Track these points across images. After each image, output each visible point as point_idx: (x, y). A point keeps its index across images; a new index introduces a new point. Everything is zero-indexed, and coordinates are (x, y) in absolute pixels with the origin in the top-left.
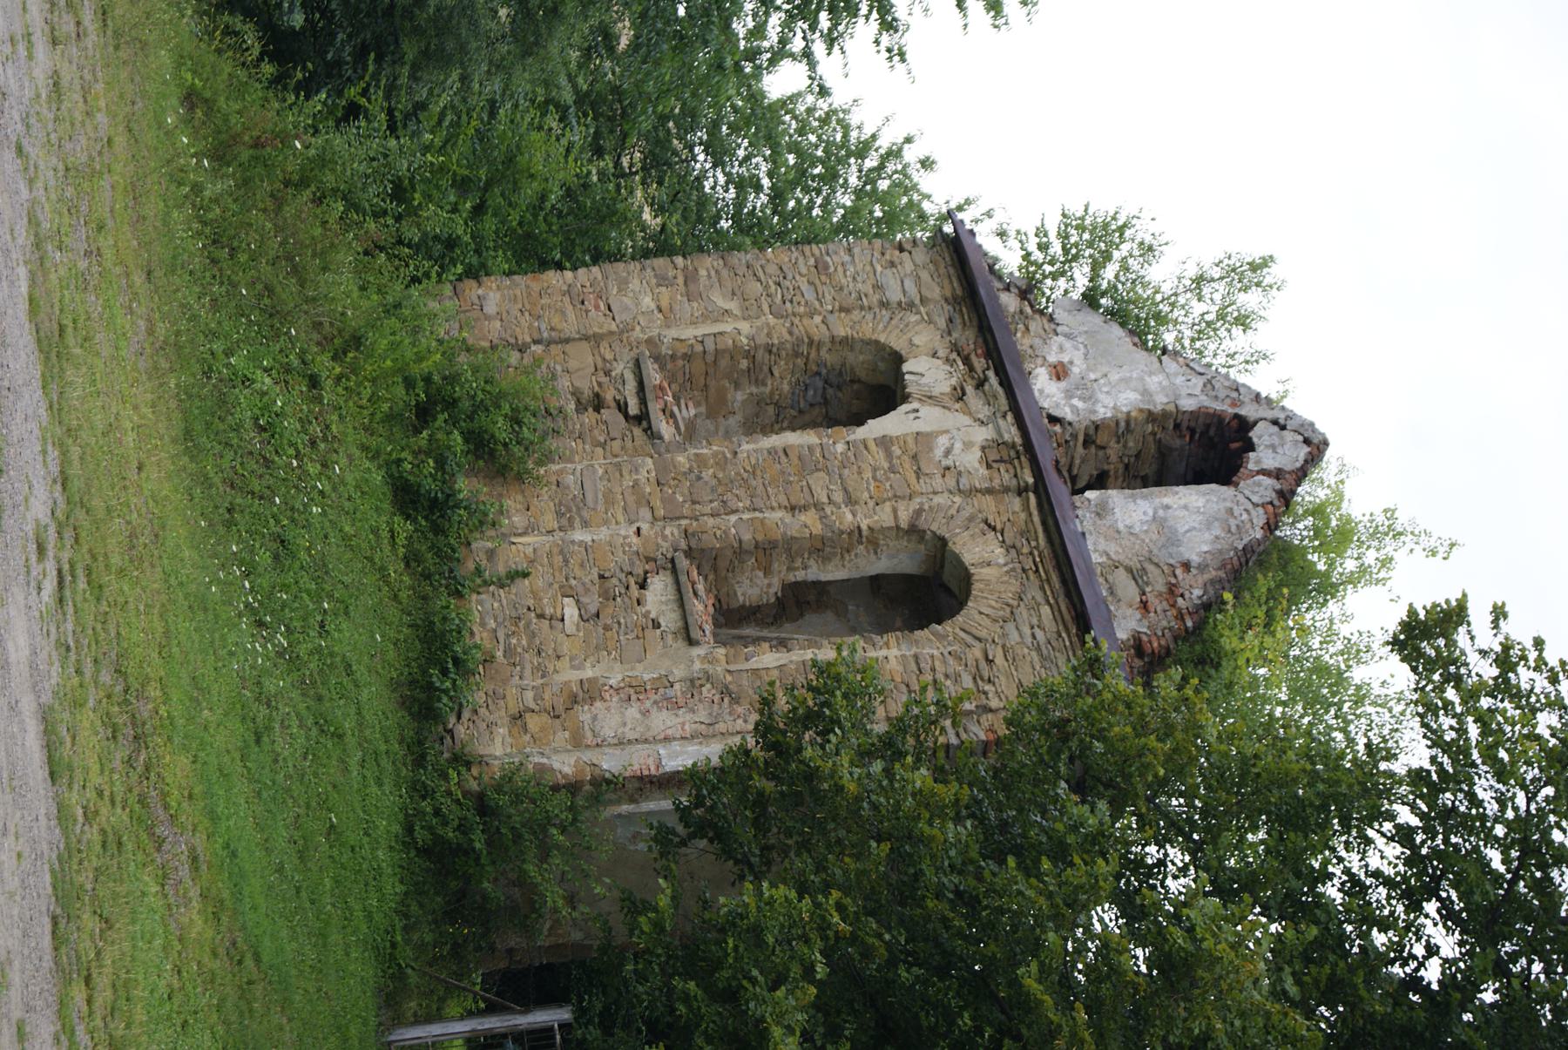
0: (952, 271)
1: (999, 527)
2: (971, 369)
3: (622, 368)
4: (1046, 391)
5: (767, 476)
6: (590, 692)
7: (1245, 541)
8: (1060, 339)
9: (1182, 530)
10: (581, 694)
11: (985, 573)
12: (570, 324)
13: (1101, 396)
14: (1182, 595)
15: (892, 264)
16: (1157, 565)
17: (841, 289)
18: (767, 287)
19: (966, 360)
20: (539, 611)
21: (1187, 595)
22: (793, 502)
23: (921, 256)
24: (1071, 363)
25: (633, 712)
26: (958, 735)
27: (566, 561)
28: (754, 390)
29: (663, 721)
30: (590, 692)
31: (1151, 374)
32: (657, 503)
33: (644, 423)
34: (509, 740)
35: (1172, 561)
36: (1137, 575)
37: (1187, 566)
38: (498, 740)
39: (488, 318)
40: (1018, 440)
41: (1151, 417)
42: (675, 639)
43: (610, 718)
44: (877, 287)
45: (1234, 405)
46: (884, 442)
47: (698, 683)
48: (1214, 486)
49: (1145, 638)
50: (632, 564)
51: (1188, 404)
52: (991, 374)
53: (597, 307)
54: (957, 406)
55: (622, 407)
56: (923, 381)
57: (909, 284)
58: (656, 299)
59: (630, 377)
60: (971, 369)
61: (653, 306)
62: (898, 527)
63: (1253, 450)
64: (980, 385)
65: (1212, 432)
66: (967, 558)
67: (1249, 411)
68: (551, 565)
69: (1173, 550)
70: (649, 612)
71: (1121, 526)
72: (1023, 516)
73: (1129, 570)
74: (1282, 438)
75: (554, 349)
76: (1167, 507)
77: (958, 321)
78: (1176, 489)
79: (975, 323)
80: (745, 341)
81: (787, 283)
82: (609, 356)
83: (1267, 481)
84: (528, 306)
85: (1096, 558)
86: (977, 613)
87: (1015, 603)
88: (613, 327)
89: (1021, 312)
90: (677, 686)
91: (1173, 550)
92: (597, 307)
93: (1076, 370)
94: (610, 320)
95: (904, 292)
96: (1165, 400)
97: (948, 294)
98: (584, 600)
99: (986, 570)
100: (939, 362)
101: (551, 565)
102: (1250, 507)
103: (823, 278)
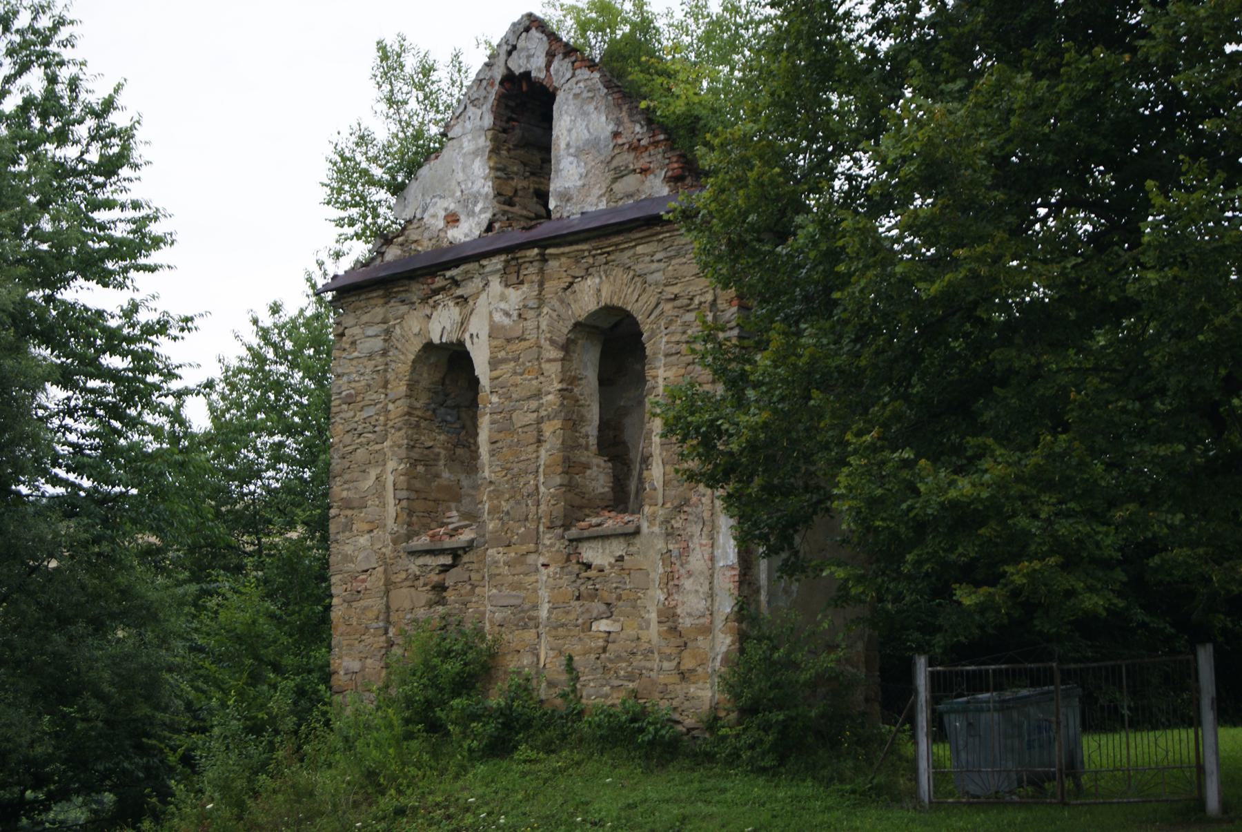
0: (363, 297)
3: (414, 566)
4: (466, 231)
6: (669, 616)
7: (601, 86)
9: (587, 135)
12: (375, 603)
13: (475, 188)
14: (639, 140)
15: (353, 343)
16: (613, 158)
17: (369, 385)
18: (361, 444)
19: (436, 292)
24: (446, 209)
25: (688, 584)
27: (563, 625)
28: (442, 462)
29: (697, 561)
30: (669, 616)
31: (461, 147)
32: (524, 548)
33: (460, 552)
35: (611, 146)
37: (616, 135)
38: (700, 693)
39: (363, 669)
40: (503, 257)
43: (691, 603)
44: (370, 357)
46: (494, 363)
47: (670, 530)
48: (555, 107)
49: (670, 173)
50: (570, 573)
51: (488, 120)
52: (448, 274)
53: (364, 581)
54: (471, 303)
55: (445, 569)
56: (448, 327)
57: (370, 332)
58: (362, 533)
59: (421, 561)
60: (443, 289)
62: (563, 359)
64: (456, 283)
65: (512, 104)
66: (593, 307)
69: (602, 144)
70: (610, 564)
71: (579, 183)
72: (563, 260)
74: (522, 49)
75: (394, 617)
76: (568, 145)
77: (403, 295)
80: (402, 466)
81: (360, 428)
82: (403, 575)
84: (357, 636)
86: (637, 305)
88: (381, 569)
89: (402, 245)
90: (671, 547)
91: (602, 144)
93: (452, 206)
94: (375, 572)
95: (376, 336)
96: (483, 138)
102: (574, 80)
103: (359, 399)
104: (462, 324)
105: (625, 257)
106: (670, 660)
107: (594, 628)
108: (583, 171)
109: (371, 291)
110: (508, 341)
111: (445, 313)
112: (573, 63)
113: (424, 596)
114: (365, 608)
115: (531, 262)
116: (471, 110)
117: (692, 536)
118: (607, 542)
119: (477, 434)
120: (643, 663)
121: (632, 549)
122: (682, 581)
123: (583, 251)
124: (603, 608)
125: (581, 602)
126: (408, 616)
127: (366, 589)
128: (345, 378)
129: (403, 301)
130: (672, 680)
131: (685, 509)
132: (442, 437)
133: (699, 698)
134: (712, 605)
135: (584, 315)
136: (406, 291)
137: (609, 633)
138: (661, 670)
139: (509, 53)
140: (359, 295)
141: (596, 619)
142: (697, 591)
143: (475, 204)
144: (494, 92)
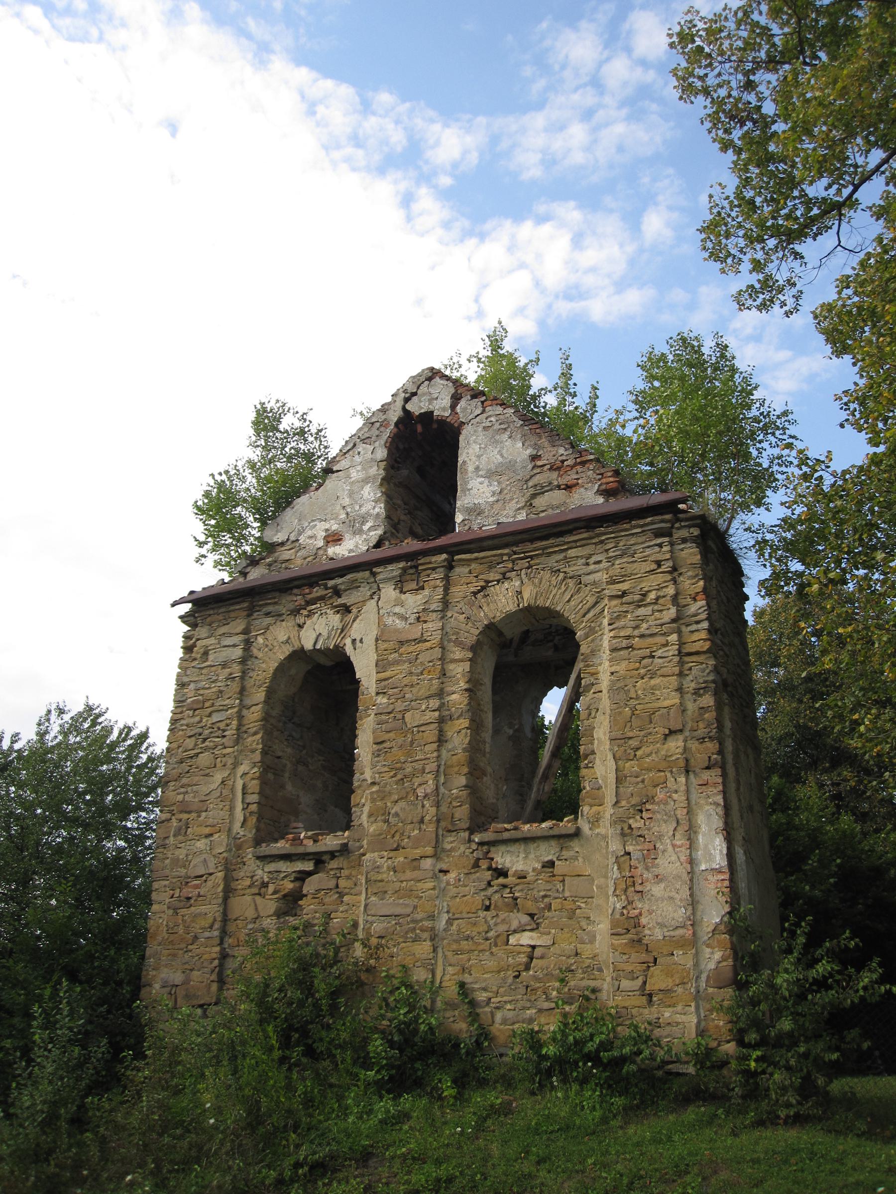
0: (223, 610)
1: (483, 584)
2: (322, 598)
3: (262, 874)
5: (402, 759)
6: (629, 927)
7: (516, 420)
8: (302, 539)
9: (500, 459)
10: (629, 936)
11: (528, 594)
12: (211, 909)
13: (364, 510)
14: (563, 462)
15: (206, 653)
16: (531, 477)
17: (221, 692)
18: (206, 749)
19: (313, 602)
20: (522, 967)
21: (564, 458)
22: (435, 739)
23: (202, 632)
24: (327, 530)
25: (657, 890)
26: (698, 622)
27: (467, 938)
28: (287, 775)
29: (671, 862)
30: (629, 927)
31: (349, 477)
32: (418, 852)
33: (325, 857)
34: (679, 1008)
35: (530, 466)
36: (539, 491)
37: (534, 458)
38: (679, 1018)
39: (186, 982)
40: (402, 565)
41: (386, 480)
42: (568, 848)
43: (663, 910)
44: (224, 665)
45: (386, 427)
46: (381, 665)
47: (627, 831)
48: (461, 438)
49: (604, 487)
50: (479, 880)
51: (382, 453)
52: (331, 583)
53: (197, 887)
54: (355, 611)
55: (302, 877)
56: (325, 634)
57: (228, 641)
58: (200, 837)
59: (272, 867)
60: (322, 598)
61: (207, 841)
62: (470, 660)
63: (432, 412)
64: (337, 593)
65: (401, 446)
66: (512, 607)
67: (395, 415)
68: (470, 951)
70: (534, 870)
72: (473, 566)
73: (534, 496)
74: (424, 394)
75: (231, 928)
76: (477, 469)
77: (270, 608)
78: (460, 460)
79: (277, 594)
80: (256, 770)
81: (207, 732)
82: (248, 882)
83: (462, 403)
84: (183, 945)
85: (522, 516)
86: (568, 604)
87: (562, 575)
88: (221, 875)
89: (270, 565)
90: (629, 848)
91: (519, 466)
92: (197, 887)
93: (335, 527)
94: (213, 877)
95: (234, 646)
96: (375, 468)
97: (245, 613)
98: (515, 925)
99: (526, 595)
100: (308, 622)
101: (470, 951)
102: (485, 415)
103: (207, 704)
104: (342, 631)
105: (552, 561)
106: (633, 979)
107: (512, 940)
108: (497, 489)
109: (232, 604)
110: (402, 643)
111: (323, 620)
112: (483, 402)
113: (269, 905)
114: (196, 916)
115: (434, 569)
116: (361, 447)
117: (660, 837)
118: (532, 846)
119: (355, 736)
120: (586, 983)
121: (566, 854)
122: (648, 886)
123: (502, 555)
124: (526, 919)
125: (493, 912)
126: (250, 926)
127: (199, 896)
128: (192, 686)
129: (267, 614)
130: (638, 1003)
131: (648, 806)
132: (289, 750)
133: (678, 1023)
134: (694, 914)
135: (499, 616)
136: (275, 603)
137: (533, 947)
138: (616, 993)
139: (407, 400)
140: (220, 607)
141: (515, 931)
142: (671, 898)
143: (363, 523)
144: (388, 431)
